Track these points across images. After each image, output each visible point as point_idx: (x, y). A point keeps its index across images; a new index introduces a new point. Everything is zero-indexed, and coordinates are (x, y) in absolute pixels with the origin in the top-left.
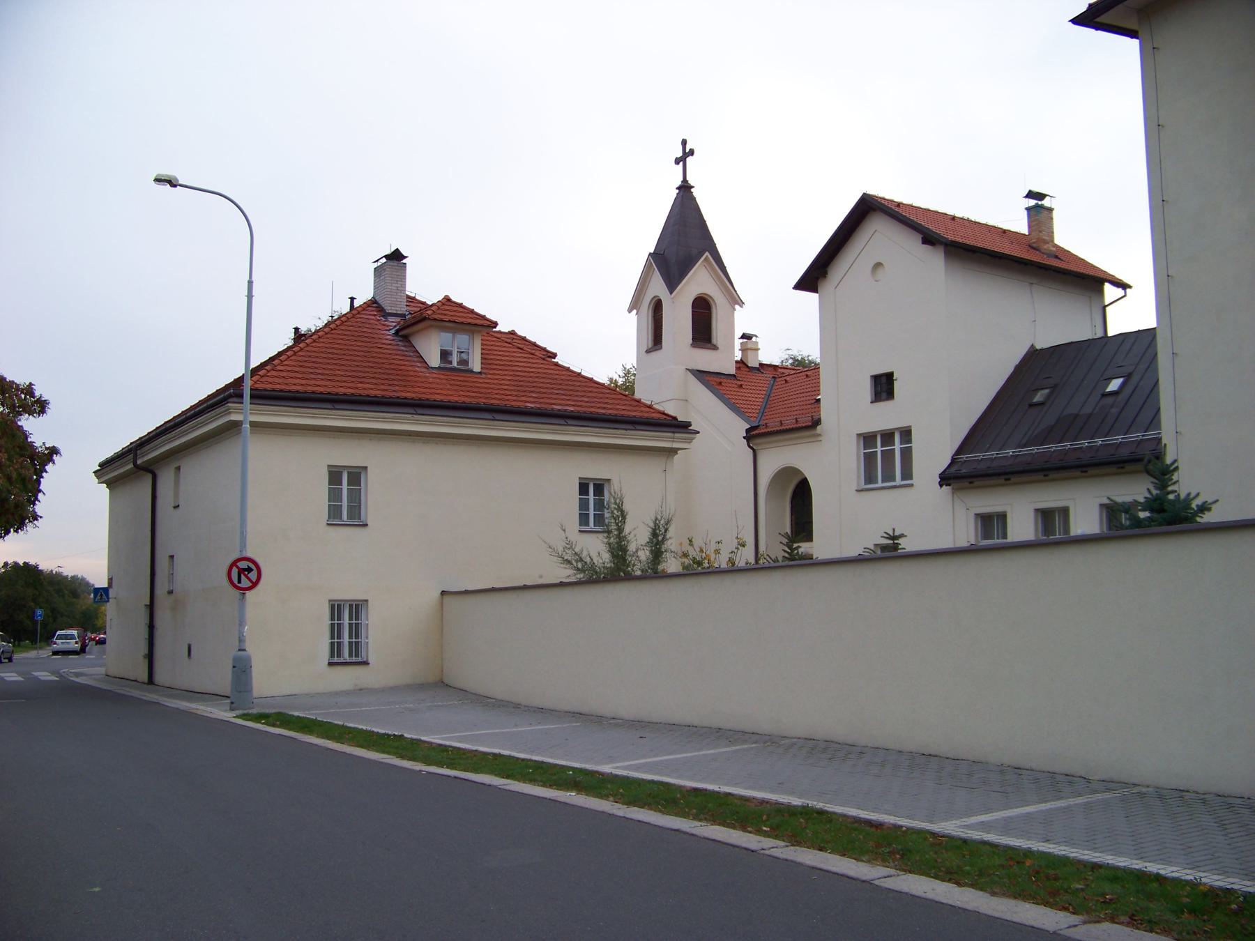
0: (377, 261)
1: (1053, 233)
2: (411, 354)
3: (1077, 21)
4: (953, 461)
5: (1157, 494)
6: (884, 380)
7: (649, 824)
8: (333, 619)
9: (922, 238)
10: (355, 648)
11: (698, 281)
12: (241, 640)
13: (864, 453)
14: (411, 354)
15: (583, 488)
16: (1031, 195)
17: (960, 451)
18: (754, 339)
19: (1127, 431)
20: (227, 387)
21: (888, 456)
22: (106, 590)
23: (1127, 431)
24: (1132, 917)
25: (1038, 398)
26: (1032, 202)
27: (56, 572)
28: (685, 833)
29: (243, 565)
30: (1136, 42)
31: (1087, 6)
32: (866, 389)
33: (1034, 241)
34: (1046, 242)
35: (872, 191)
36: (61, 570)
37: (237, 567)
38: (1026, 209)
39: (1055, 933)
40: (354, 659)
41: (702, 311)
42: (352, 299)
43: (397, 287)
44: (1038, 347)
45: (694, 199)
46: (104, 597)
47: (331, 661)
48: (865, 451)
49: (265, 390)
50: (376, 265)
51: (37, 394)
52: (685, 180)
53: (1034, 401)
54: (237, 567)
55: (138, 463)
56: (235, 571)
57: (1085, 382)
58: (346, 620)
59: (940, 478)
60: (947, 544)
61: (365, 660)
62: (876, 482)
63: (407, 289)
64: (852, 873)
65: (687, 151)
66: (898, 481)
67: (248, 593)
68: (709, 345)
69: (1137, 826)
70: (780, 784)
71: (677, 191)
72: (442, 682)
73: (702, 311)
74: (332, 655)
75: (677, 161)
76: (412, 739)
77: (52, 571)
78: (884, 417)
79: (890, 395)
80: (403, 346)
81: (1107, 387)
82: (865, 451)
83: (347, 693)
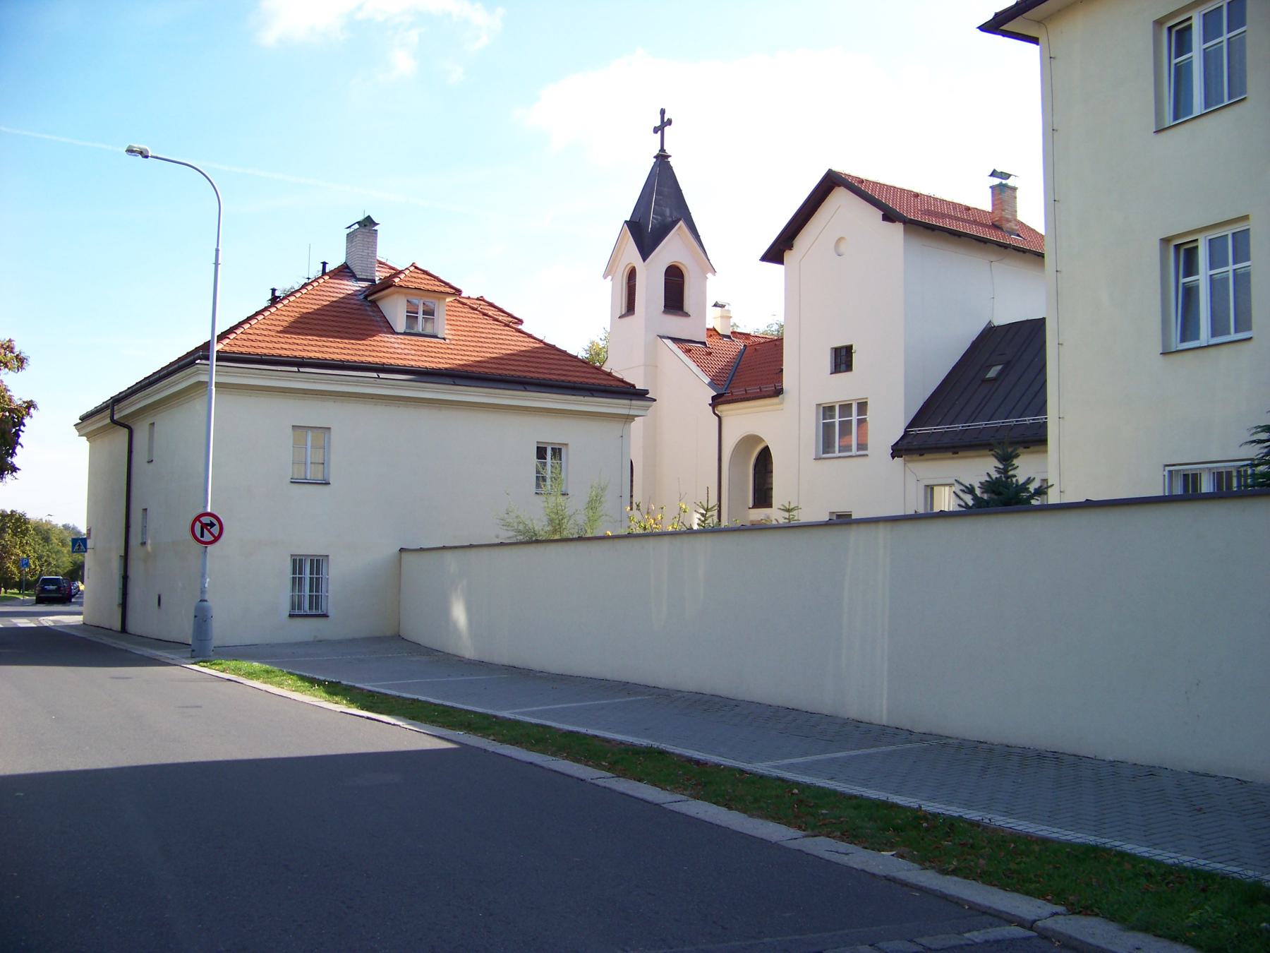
0: (350, 227)
1: (1016, 211)
2: (378, 319)
3: (984, 28)
4: (906, 433)
5: (996, 478)
6: (844, 352)
7: (511, 758)
8: (294, 573)
9: (883, 215)
10: (315, 601)
11: (671, 250)
12: (203, 591)
13: (866, 415)
14: (378, 319)
15: (541, 453)
16: (994, 174)
17: (911, 425)
18: (726, 308)
19: (1008, 415)
20: (197, 349)
21: (845, 427)
22: (84, 541)
23: (1008, 415)
24: (843, 834)
25: (992, 373)
26: (996, 181)
27: (46, 521)
28: (536, 765)
29: (206, 520)
30: (1033, 49)
31: (993, 15)
32: (827, 361)
33: (997, 219)
34: (1008, 221)
35: (836, 168)
36: (51, 518)
37: (200, 522)
38: (991, 187)
39: (776, 843)
40: (314, 612)
41: (675, 282)
42: (324, 264)
43: (368, 253)
44: (996, 323)
45: (671, 168)
46: (82, 547)
47: (292, 613)
48: (824, 421)
49: (242, 353)
50: (348, 231)
51: (17, 350)
52: (662, 149)
53: (987, 377)
54: (200, 522)
55: (115, 418)
56: (198, 525)
57: (1036, 360)
58: (307, 574)
59: (892, 449)
60: (899, 512)
61: (325, 612)
62: (834, 452)
63: (378, 254)
64: (650, 798)
65: (665, 120)
66: (854, 451)
67: (210, 548)
68: (681, 312)
69: (1145, 793)
70: (646, 729)
71: (655, 160)
72: (399, 636)
73: (675, 282)
74: (293, 608)
75: (656, 130)
76: (346, 685)
77: (41, 519)
78: (842, 388)
79: (849, 367)
80: (371, 311)
81: (986, 374)
82: (824, 421)
83: (306, 644)
